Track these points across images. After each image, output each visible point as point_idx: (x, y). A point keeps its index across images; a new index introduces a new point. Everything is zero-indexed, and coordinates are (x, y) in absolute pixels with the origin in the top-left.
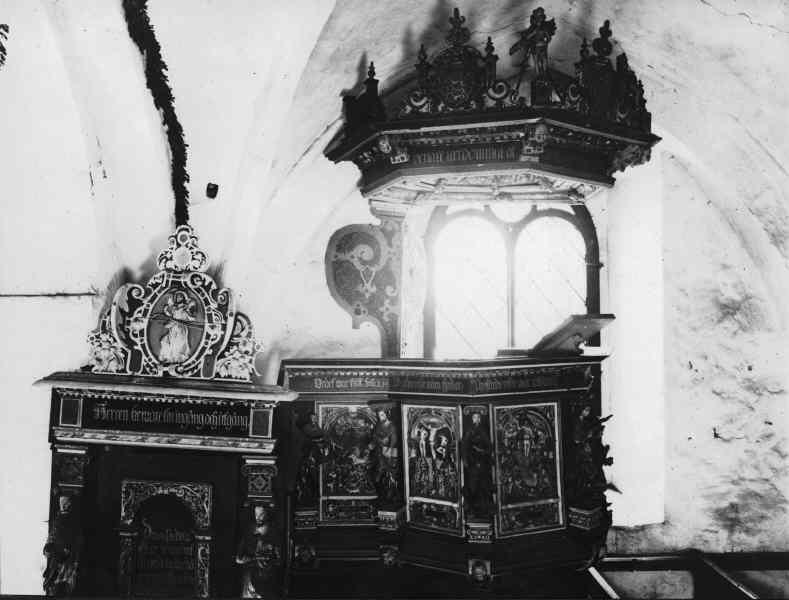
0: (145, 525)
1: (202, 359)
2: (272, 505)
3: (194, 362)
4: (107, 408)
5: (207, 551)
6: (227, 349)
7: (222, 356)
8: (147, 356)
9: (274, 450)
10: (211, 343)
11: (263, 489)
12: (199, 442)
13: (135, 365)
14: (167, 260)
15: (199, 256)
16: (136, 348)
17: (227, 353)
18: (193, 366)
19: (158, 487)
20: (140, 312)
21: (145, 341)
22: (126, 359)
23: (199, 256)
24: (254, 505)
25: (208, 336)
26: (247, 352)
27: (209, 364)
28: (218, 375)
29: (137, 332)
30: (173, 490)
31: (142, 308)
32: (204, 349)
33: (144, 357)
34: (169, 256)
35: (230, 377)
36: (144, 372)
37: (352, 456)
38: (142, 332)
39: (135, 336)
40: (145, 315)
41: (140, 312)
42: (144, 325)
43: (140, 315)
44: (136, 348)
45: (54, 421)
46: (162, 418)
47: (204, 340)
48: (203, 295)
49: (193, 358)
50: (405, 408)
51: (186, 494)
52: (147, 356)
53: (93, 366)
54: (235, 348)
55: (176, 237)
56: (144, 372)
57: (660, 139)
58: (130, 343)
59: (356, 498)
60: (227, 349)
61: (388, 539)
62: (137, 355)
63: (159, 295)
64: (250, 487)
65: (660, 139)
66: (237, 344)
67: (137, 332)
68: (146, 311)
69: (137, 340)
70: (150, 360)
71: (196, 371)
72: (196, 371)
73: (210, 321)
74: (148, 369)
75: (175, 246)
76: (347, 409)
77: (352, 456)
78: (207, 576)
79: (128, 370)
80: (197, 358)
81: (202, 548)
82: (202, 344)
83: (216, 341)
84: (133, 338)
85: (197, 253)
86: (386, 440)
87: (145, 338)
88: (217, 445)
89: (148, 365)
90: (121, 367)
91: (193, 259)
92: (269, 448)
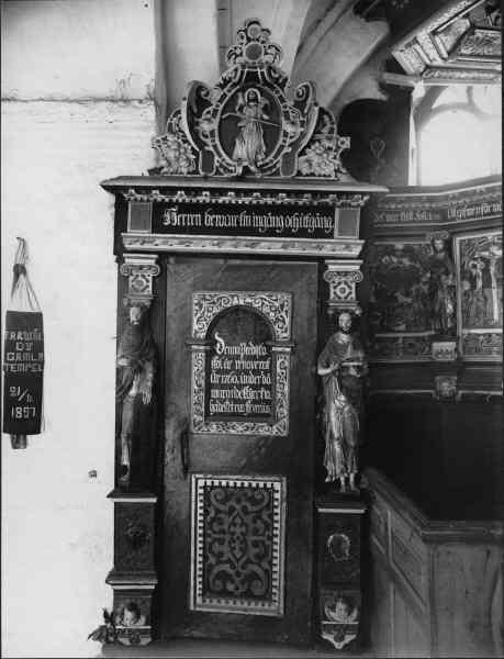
0: (217, 338)
1: (280, 158)
2: (357, 312)
3: (272, 161)
4: (178, 213)
5: (287, 364)
6: (308, 146)
7: (303, 153)
8: (220, 156)
9: (361, 253)
10: (289, 141)
11: (346, 298)
12: (280, 245)
13: (208, 165)
14: (237, 56)
15: (273, 50)
16: (206, 148)
17: (308, 150)
18: (271, 165)
19: (233, 297)
20: (208, 112)
21: (217, 142)
22: (197, 160)
23: (273, 50)
24: (338, 313)
25: (286, 134)
26: (330, 149)
27: (288, 159)
28: (299, 173)
29: (208, 133)
30: (248, 300)
31: (210, 109)
32: (282, 147)
33: (216, 158)
34: (238, 52)
35: (312, 174)
36: (218, 172)
37: (398, 294)
38: (212, 132)
39: (207, 137)
40: (214, 116)
41: (208, 112)
42: (215, 125)
43: (209, 116)
44: (206, 148)
45: (120, 226)
46: (238, 223)
47: (281, 139)
48: (277, 92)
49: (270, 158)
50: (457, 240)
51: (263, 304)
52: (220, 156)
53: (162, 168)
54: (317, 144)
55: (245, 31)
56: (218, 172)
57: (108, 496)
58: (202, 145)
59: (403, 335)
60: (308, 146)
61: (444, 368)
62: (209, 156)
63: (229, 95)
64: (332, 296)
65: (108, 496)
66: (319, 141)
67: (208, 133)
68: (215, 111)
69: (208, 141)
70: (223, 160)
71: (274, 170)
72: (274, 170)
73: (287, 118)
74: (222, 170)
75: (245, 41)
76: (393, 246)
77: (398, 294)
78: (286, 389)
79: (200, 170)
80: (275, 157)
81: (280, 360)
82: (280, 142)
83: (294, 140)
84: (202, 138)
85: (269, 47)
86: (443, 270)
87: (217, 139)
88: (298, 247)
89: (221, 166)
90: (192, 169)
91: (266, 54)
92: (356, 251)
